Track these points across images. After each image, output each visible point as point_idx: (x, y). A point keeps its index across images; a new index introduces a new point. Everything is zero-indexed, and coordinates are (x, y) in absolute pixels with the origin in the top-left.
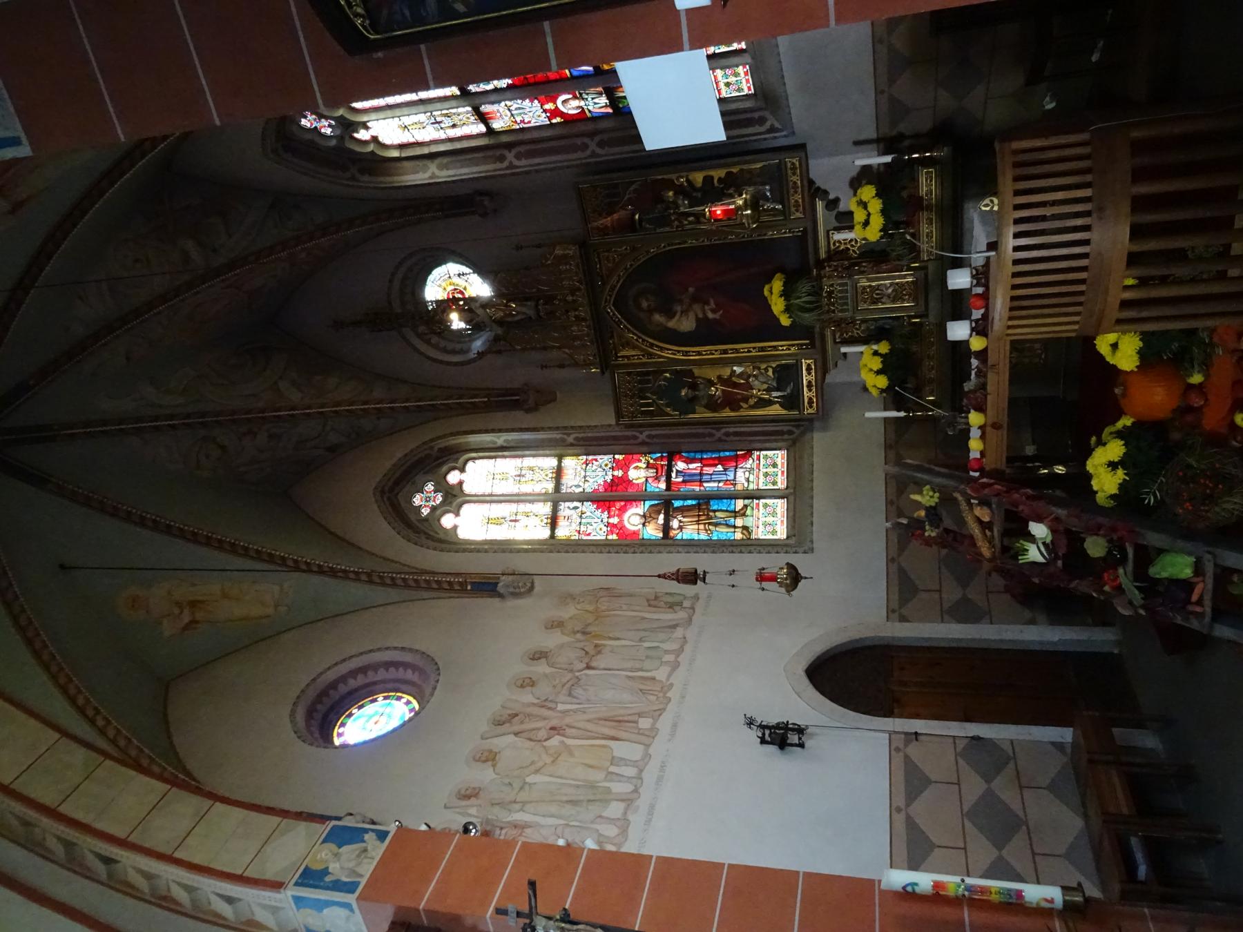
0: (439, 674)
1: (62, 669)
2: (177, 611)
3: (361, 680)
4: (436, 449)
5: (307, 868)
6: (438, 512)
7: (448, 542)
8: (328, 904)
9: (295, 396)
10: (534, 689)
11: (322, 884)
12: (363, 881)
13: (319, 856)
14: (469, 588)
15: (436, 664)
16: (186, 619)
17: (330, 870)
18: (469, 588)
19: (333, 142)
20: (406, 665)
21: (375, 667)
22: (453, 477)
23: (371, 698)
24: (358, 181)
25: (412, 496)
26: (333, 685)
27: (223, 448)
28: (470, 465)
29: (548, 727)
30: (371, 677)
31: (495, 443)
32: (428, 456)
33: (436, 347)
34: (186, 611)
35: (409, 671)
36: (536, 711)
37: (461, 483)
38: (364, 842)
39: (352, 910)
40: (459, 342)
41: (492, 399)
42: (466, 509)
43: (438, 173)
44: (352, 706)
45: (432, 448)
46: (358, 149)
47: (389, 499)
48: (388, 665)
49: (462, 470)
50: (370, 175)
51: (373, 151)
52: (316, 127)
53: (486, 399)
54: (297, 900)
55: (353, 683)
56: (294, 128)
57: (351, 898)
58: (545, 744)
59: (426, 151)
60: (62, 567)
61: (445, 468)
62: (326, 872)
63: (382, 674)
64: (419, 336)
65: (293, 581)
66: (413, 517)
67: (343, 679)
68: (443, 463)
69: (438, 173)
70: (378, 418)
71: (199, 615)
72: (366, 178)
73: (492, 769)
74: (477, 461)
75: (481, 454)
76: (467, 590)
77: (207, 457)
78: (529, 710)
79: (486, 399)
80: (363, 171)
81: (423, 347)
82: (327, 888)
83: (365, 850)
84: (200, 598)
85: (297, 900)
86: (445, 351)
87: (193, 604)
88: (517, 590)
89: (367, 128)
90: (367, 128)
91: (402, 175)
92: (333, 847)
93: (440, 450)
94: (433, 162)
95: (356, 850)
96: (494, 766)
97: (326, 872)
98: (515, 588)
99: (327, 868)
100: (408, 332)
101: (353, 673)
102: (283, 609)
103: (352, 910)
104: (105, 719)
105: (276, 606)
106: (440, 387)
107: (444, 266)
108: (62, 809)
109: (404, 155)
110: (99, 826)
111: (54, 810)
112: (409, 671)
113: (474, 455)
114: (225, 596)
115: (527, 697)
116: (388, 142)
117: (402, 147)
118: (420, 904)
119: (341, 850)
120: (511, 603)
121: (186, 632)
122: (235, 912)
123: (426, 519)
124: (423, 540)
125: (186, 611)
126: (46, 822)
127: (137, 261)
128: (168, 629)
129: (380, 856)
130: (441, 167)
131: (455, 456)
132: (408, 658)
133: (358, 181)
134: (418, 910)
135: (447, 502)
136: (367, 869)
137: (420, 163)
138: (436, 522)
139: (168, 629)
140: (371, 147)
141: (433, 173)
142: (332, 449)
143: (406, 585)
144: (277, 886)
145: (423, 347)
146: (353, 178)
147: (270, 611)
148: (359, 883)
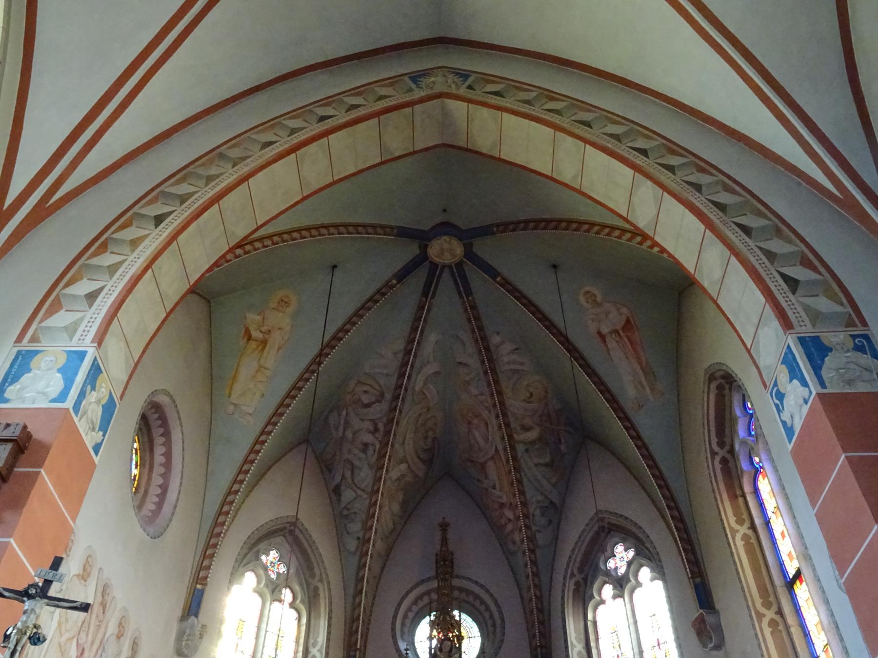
0: (151, 538)
1: (283, 241)
2: (264, 329)
3: (159, 459)
4: (320, 585)
5: (101, 372)
6: (261, 572)
7: (235, 575)
8: (68, 383)
9: (395, 474)
10: (115, 636)
11: (88, 381)
12: (76, 419)
13: (104, 385)
14: (199, 587)
15: (159, 537)
16: (255, 334)
17: (93, 392)
18: (199, 587)
19: (603, 567)
20: (160, 505)
21: (166, 475)
22: (287, 595)
23: (139, 464)
24: (571, 578)
25: (278, 550)
26: (167, 434)
27: (368, 406)
28: (294, 614)
29: (85, 646)
30: (158, 470)
31: (314, 646)
32: (313, 576)
33: (409, 609)
34: (261, 336)
35: (153, 507)
36: (100, 636)
37: (280, 601)
38: (98, 431)
39: (54, 401)
40: (409, 631)
41: (358, 652)
42: (259, 600)
43: (576, 650)
44: (140, 445)
45: (321, 580)
46: (596, 586)
47: (285, 528)
48: (164, 488)
49: (292, 605)
50: (574, 590)
51: (594, 597)
52: (615, 556)
53: (358, 647)
54: (82, 355)
55: (159, 450)
56: (616, 539)
57: (69, 404)
58: (76, 638)
59: (593, 644)
60: (335, 267)
61: (297, 588)
62: (93, 388)
63: (157, 480)
64: (428, 593)
65: (255, 426)
66: (262, 546)
67: (168, 444)
68: (301, 585)
69: (576, 650)
70: (358, 538)
71: (253, 345)
72: (572, 587)
73: (77, 573)
74: (296, 622)
75: (303, 628)
76: (197, 583)
77: (365, 392)
78: (102, 630)
79: (358, 647)
80: (577, 584)
81: (412, 596)
82: (84, 386)
83: (93, 430)
84: (266, 351)
85: (82, 355)
86: (405, 616)
87: (264, 343)
88: (185, 638)
89: (615, 597)
90: (615, 597)
91: (574, 617)
92: (104, 401)
93: (316, 589)
94: (583, 648)
95: (97, 420)
96: (78, 576)
97: (93, 388)
98: (189, 635)
99: (95, 391)
100: (434, 584)
101: (168, 455)
102: (232, 408)
103: (54, 401)
104: (239, 256)
105: (235, 405)
106: (373, 604)
107: (479, 634)
108: (216, 206)
109: (589, 623)
110: (194, 225)
111: (218, 201)
112: (153, 507)
113: (304, 620)
114: (261, 368)
115: (112, 628)
116: (599, 611)
117: (595, 623)
118: (44, 470)
119: (101, 406)
120: (175, 626)
121: (244, 330)
122: (75, 297)
123: (258, 558)
124: (245, 551)
125: (261, 336)
126: (211, 193)
127: (531, 395)
128: (253, 318)
129: (85, 440)
130: (579, 653)
131: (306, 600)
132: (167, 509)
133: (571, 578)
134: (41, 467)
135: (269, 584)
136: (82, 426)
137: (582, 636)
138: (253, 568)
139: (253, 318)
140: (597, 597)
141: (576, 647)
142: (337, 491)
143: (216, 524)
144: (100, 340)
145: (412, 596)
146: (573, 575)
147: (234, 398)
148: (77, 416)
